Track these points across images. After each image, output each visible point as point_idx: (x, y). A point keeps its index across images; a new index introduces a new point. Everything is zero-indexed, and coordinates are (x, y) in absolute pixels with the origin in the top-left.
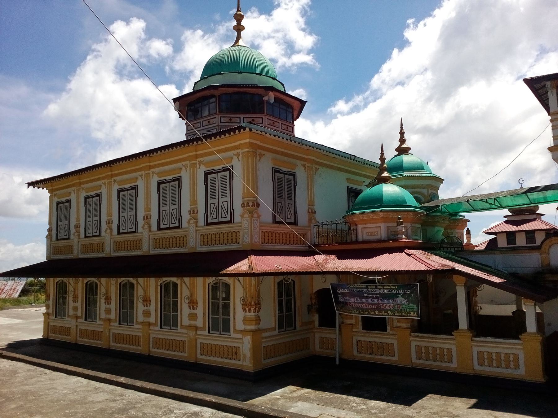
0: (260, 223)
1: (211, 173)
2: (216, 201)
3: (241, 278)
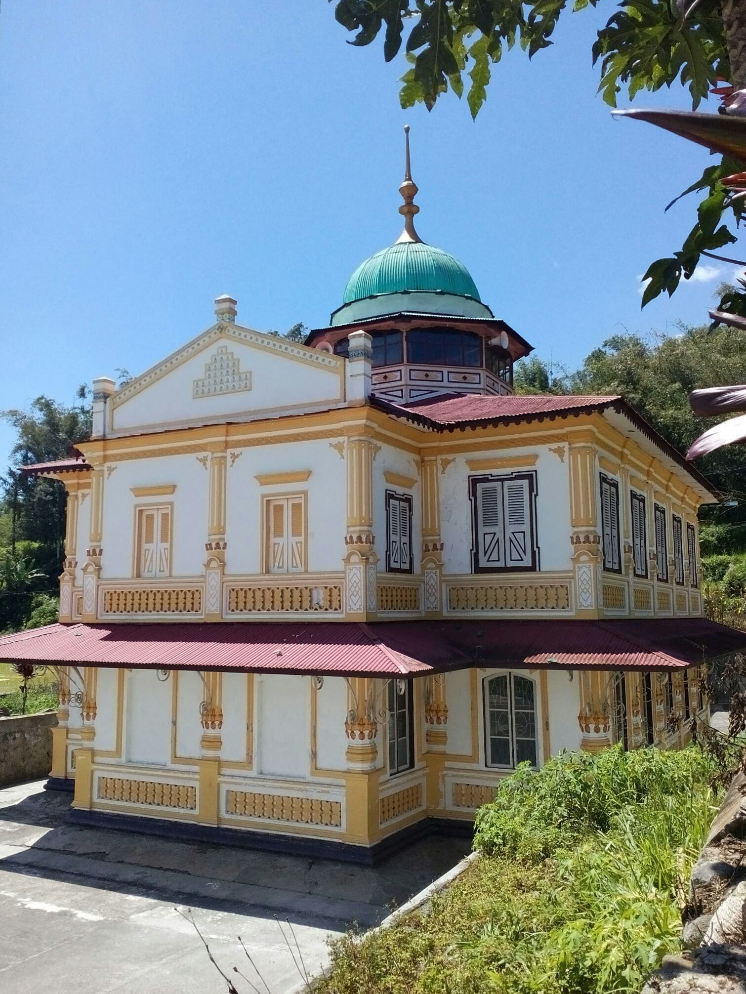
0: (441, 575)
1: (485, 480)
2: (498, 530)
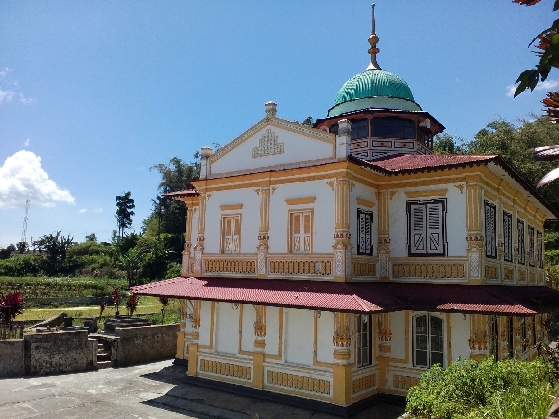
3: (192, 301)
